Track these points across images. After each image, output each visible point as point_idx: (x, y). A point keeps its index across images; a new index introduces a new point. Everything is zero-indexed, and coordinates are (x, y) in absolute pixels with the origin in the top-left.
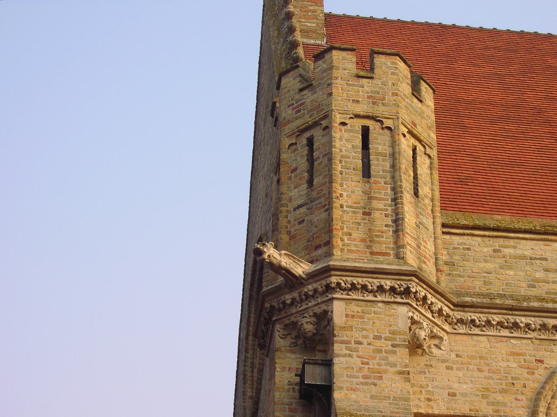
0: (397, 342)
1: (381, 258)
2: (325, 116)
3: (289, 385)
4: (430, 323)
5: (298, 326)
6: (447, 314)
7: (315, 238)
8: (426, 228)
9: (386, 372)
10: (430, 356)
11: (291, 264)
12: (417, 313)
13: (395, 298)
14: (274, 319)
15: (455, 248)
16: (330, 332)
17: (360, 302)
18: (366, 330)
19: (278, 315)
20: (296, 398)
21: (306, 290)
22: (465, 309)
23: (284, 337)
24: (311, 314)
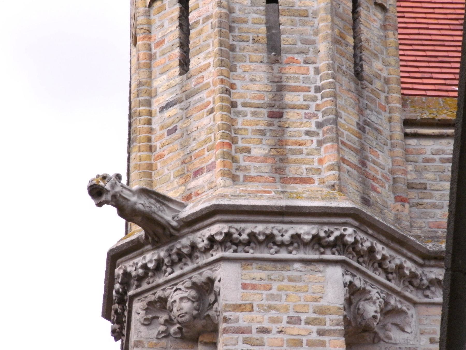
0: (327, 327)
1: (299, 188)
4: (383, 289)
5: (168, 305)
6: (411, 272)
7: (193, 158)
8: (377, 129)
10: (386, 343)
11: (153, 206)
12: (358, 276)
14: (130, 293)
15: (427, 160)
16: (218, 313)
17: (265, 263)
18: (274, 308)
19: (138, 286)
21: (179, 246)
23: (146, 323)
24: (188, 284)
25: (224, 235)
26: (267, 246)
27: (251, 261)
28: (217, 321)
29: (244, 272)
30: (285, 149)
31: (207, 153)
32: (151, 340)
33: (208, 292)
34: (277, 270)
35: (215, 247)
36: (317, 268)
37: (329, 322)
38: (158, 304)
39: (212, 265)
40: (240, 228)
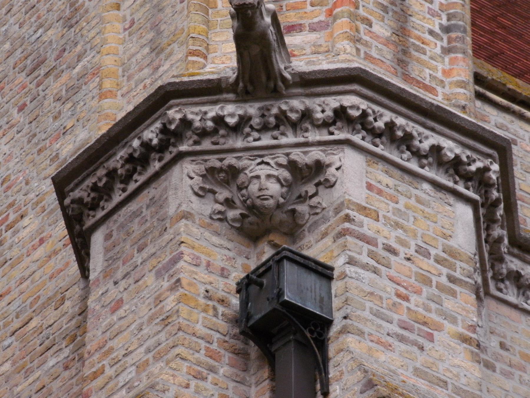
3: (206, 297)
9: (439, 328)
13: (456, 182)
19: (196, 143)
20: (220, 330)
22: (526, 255)
23: (201, 193)
24: (283, 160)
25: (361, 111)
26: (398, 148)
27: (378, 159)
28: (305, 222)
29: (370, 169)
30: (408, 40)
31: (309, 8)
32: (203, 216)
33: (303, 181)
34: (404, 182)
35: (339, 124)
36: (447, 199)
37: (460, 269)
38: (222, 175)
39: (327, 146)
40: (378, 111)
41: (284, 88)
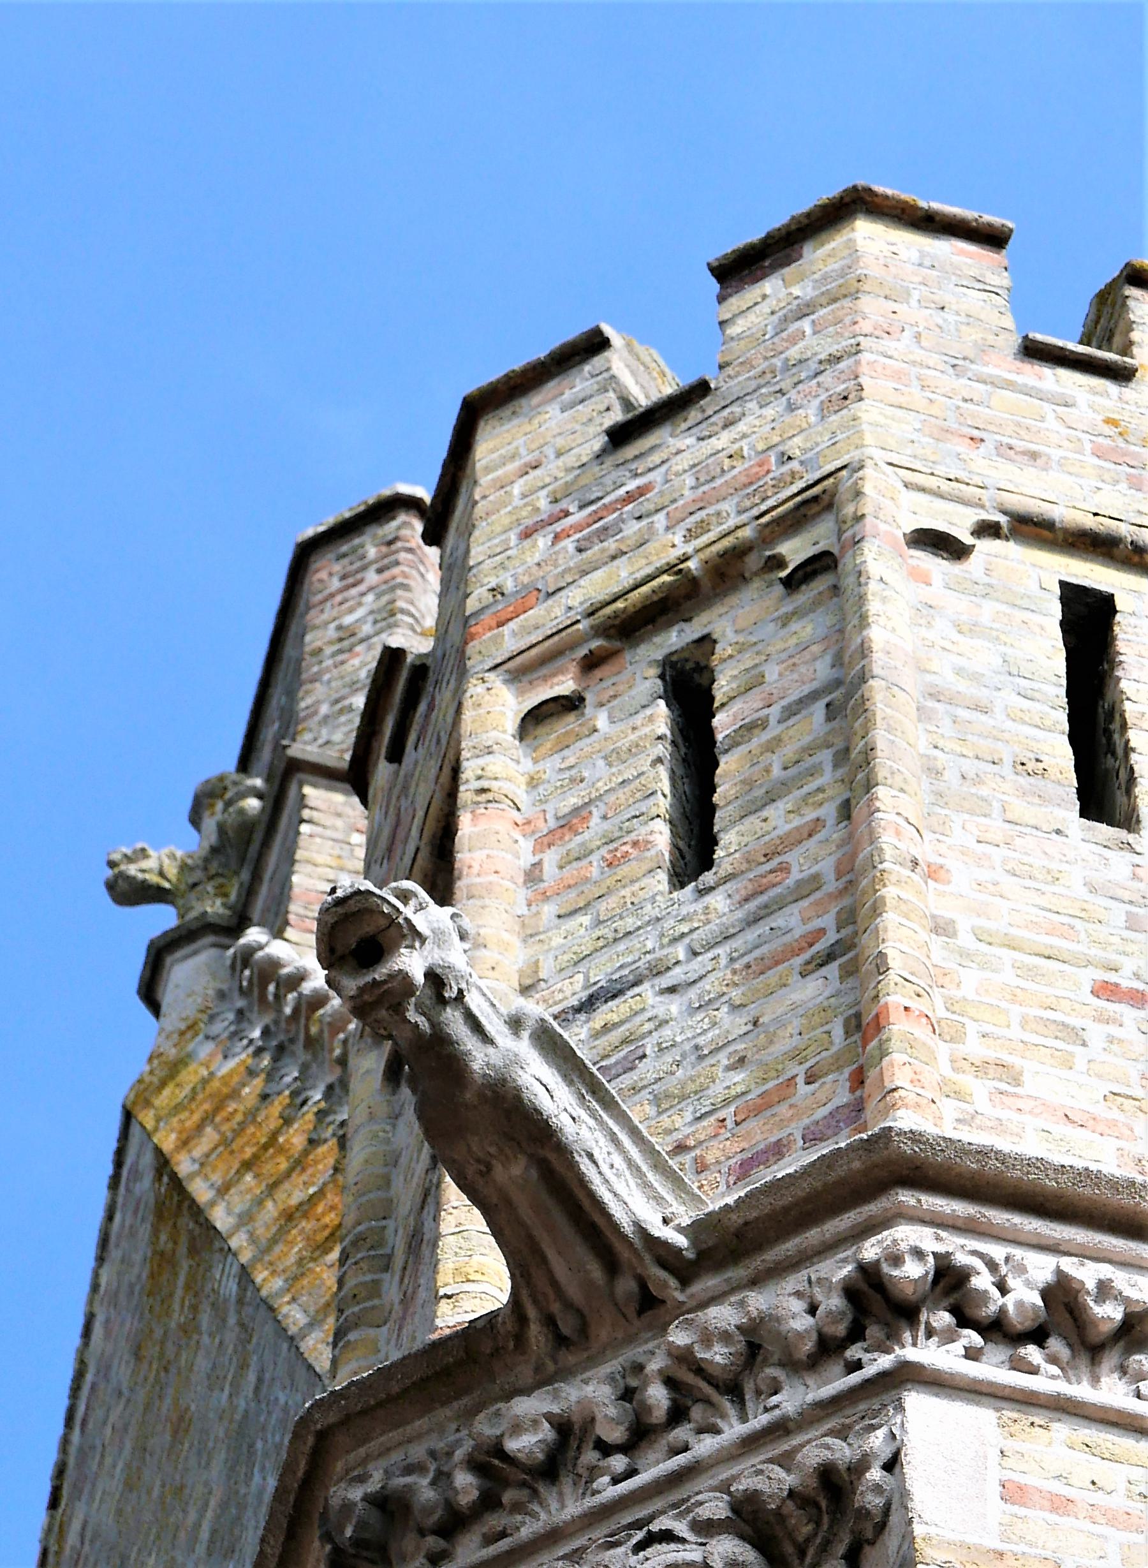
2: (805, 503)
24: (716, 1508)
35: (874, 1331)
41: (673, 1282)
